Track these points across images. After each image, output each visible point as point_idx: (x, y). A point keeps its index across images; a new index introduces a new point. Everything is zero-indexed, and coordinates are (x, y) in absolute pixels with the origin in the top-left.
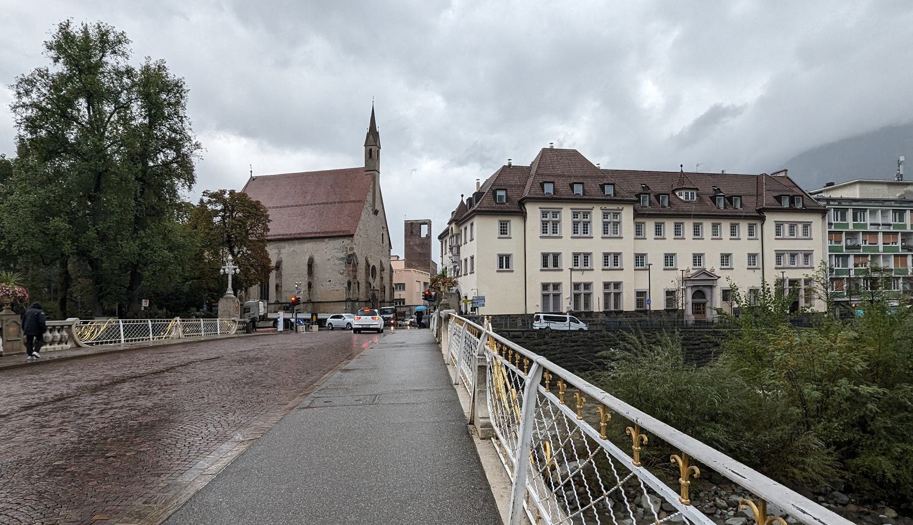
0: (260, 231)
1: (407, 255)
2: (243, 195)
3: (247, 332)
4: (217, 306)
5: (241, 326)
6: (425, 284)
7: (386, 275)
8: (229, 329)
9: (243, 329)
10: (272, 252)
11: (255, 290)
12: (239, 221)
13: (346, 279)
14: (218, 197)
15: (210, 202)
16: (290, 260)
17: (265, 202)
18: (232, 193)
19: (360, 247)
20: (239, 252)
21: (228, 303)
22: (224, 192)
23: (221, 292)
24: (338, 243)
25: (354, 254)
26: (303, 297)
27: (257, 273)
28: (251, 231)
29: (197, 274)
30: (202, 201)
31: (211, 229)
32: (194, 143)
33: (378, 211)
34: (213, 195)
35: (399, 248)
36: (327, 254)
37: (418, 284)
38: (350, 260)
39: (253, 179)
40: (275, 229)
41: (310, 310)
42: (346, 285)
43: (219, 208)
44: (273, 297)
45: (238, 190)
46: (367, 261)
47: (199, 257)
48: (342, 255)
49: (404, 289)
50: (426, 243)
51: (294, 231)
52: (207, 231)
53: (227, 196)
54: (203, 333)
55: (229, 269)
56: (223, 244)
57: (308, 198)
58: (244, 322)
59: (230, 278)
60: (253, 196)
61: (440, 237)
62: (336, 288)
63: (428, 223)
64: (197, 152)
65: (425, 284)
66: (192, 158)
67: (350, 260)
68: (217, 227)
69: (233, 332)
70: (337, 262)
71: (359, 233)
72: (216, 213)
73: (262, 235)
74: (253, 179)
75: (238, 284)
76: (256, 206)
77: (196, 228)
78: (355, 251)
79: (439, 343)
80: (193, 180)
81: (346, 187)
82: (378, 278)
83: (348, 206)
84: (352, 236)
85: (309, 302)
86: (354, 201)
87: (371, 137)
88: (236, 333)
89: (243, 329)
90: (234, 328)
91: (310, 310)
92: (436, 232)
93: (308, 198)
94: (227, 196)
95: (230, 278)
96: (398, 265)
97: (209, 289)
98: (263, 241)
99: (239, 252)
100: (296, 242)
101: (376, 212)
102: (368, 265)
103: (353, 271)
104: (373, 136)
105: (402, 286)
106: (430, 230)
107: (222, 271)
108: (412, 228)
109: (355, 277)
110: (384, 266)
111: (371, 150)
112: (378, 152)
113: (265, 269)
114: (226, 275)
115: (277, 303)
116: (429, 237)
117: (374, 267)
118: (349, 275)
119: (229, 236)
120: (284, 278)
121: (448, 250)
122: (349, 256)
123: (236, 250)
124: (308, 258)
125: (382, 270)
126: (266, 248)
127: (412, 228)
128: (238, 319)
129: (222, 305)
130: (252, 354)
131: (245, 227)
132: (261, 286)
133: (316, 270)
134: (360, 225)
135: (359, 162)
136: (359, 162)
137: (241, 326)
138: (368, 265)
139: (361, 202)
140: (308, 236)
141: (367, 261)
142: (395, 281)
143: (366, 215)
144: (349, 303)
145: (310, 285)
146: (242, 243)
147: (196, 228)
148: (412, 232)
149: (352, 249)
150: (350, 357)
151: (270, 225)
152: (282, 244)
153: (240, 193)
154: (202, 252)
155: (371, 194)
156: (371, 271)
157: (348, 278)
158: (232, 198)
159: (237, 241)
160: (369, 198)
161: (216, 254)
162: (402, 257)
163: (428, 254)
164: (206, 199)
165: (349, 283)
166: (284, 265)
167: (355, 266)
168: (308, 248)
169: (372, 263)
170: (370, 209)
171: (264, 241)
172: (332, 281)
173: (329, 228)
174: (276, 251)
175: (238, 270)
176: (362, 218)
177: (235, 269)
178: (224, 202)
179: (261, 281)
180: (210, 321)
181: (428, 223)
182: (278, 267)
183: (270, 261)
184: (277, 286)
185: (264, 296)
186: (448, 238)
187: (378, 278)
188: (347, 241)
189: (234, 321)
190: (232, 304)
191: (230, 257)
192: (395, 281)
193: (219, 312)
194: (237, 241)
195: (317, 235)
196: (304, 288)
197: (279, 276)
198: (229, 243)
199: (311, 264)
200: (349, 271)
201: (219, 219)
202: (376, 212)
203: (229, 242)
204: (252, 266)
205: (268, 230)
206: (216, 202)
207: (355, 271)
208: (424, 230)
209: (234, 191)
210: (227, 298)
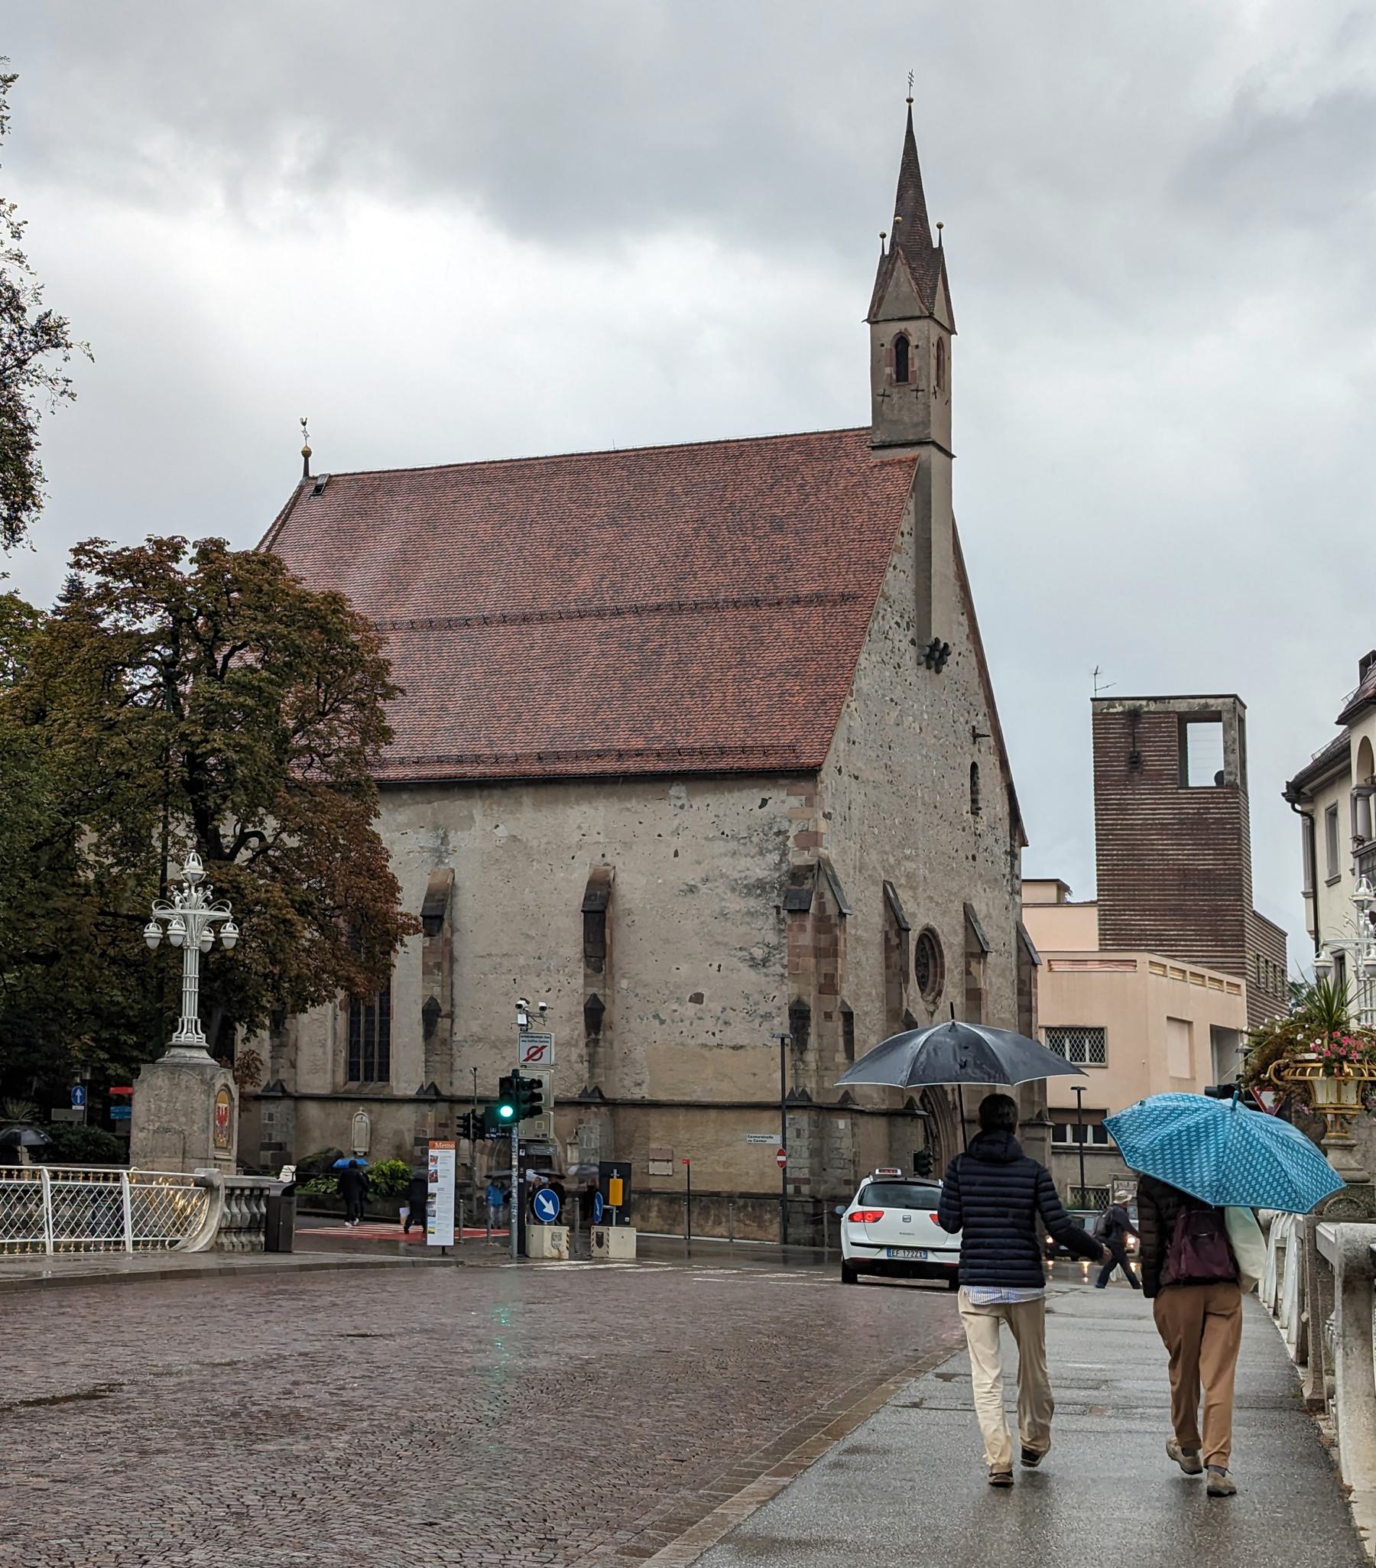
0: (344, 739)
1: (1105, 883)
2: (263, 563)
3: (271, 1247)
4: (127, 1101)
5: (241, 1211)
6: (1221, 1036)
7: (997, 979)
8: (182, 1223)
9: (253, 1227)
10: (404, 839)
11: (320, 1032)
12: (241, 688)
13: (785, 994)
14: (143, 570)
15: (105, 595)
16: (497, 884)
17: (360, 591)
18: (211, 552)
19: (864, 826)
20: (242, 840)
21: (180, 1095)
22: (172, 548)
23: (152, 1034)
24: (739, 807)
25: (819, 869)
26: (557, 1071)
27: (334, 934)
28: (299, 741)
29: (43, 936)
30: (75, 589)
31: (111, 726)
32: (31, 319)
33: (946, 649)
34: (124, 565)
35: (1063, 840)
36: (686, 861)
37: (1176, 1039)
38: (803, 894)
39: (315, 488)
40: (419, 730)
41: (562, 1166)
42: (782, 1023)
43: (150, 624)
44: (408, 1068)
45: (244, 539)
46: (891, 905)
47: (55, 855)
48: (761, 868)
49: (1099, 1055)
50: (1223, 811)
51: (519, 743)
52: (90, 732)
53: (185, 568)
54: (48, 1238)
55: (190, 922)
56: (164, 797)
57: (585, 581)
58: (256, 1194)
59: (191, 968)
60: (307, 571)
61: (1299, 792)
62: (731, 1036)
63: (1226, 713)
64: (46, 361)
65: (1221, 1036)
66: (26, 392)
67: (803, 894)
68: (142, 716)
69: (201, 1236)
70: (737, 904)
71: (850, 753)
72: (136, 647)
73: (354, 757)
74: (315, 488)
75: (234, 996)
76: (325, 616)
77: (40, 716)
78: (829, 850)
79: (1318, 1406)
80: (29, 491)
81: (778, 526)
82: (953, 991)
83: (783, 625)
84: (810, 773)
85: (592, 1099)
86: (818, 599)
87: (902, 271)
88: (216, 1248)
89: (253, 1227)
90: (207, 1222)
91: (562, 1166)
92: (1281, 749)
93: (585, 581)
94: (185, 568)
95: (191, 968)
96: (1065, 932)
97: (96, 1011)
98: (357, 788)
99: (242, 840)
100: (527, 797)
101: (935, 656)
102: (896, 922)
103: (819, 953)
104: (912, 269)
105: (1085, 1043)
106: (1236, 747)
107: (152, 931)
108: (1135, 740)
109: (829, 985)
110: (988, 931)
111: (902, 342)
112: (942, 351)
113: (368, 930)
114: (171, 952)
115: (430, 1096)
116: (1232, 785)
117: (929, 939)
118: (794, 972)
119: (194, 763)
120: (466, 971)
121: (1347, 861)
122: (798, 875)
123: (228, 828)
124: (581, 877)
125: (976, 951)
126: (377, 826)
127: (1135, 740)
128: (227, 1176)
129: (154, 1100)
130: (265, 1390)
131: (272, 720)
132: (353, 1004)
133: (632, 942)
134: (854, 719)
135: (845, 401)
136: (845, 401)
137: (241, 1211)
138: (896, 922)
139: (853, 602)
140: (584, 768)
141: (891, 905)
142: (1050, 1011)
143: (882, 666)
144: (802, 1120)
145: (595, 1015)
146: (259, 795)
147: (40, 716)
148: (1135, 761)
149: (810, 839)
150: (790, 1454)
151: (395, 714)
152: (456, 807)
153: (245, 557)
154: (71, 835)
155: (903, 561)
156: (915, 957)
157: (788, 991)
158: (211, 578)
159: (231, 784)
160: (899, 582)
161: (134, 841)
162: (1085, 886)
163: (1234, 880)
164: (91, 580)
165: (799, 1015)
166: (467, 908)
167: (831, 924)
168: (584, 832)
169: (919, 916)
170: (902, 639)
171: (363, 789)
172: (706, 1009)
173: (701, 732)
174: (425, 839)
175: (230, 932)
176: (863, 683)
177: (215, 925)
178: (174, 597)
179: (349, 984)
180: (82, 1177)
181: (1226, 713)
182: (436, 917)
183: (391, 887)
184: (431, 1014)
185: (368, 1055)
186: (1342, 798)
187: (953, 991)
188: (783, 801)
189: (208, 1187)
190: (199, 1099)
191: (194, 867)
192: (1050, 1011)
193: (137, 1138)
194: (231, 784)
195: (632, 765)
196: (565, 1027)
197: (442, 962)
198: (198, 792)
199: (598, 909)
200: (796, 951)
201: (146, 675)
202: (935, 656)
203: (193, 786)
204: (304, 908)
205: (386, 735)
206: (133, 597)
207: (828, 951)
208: (1205, 753)
209: (219, 545)
210: (177, 1067)
